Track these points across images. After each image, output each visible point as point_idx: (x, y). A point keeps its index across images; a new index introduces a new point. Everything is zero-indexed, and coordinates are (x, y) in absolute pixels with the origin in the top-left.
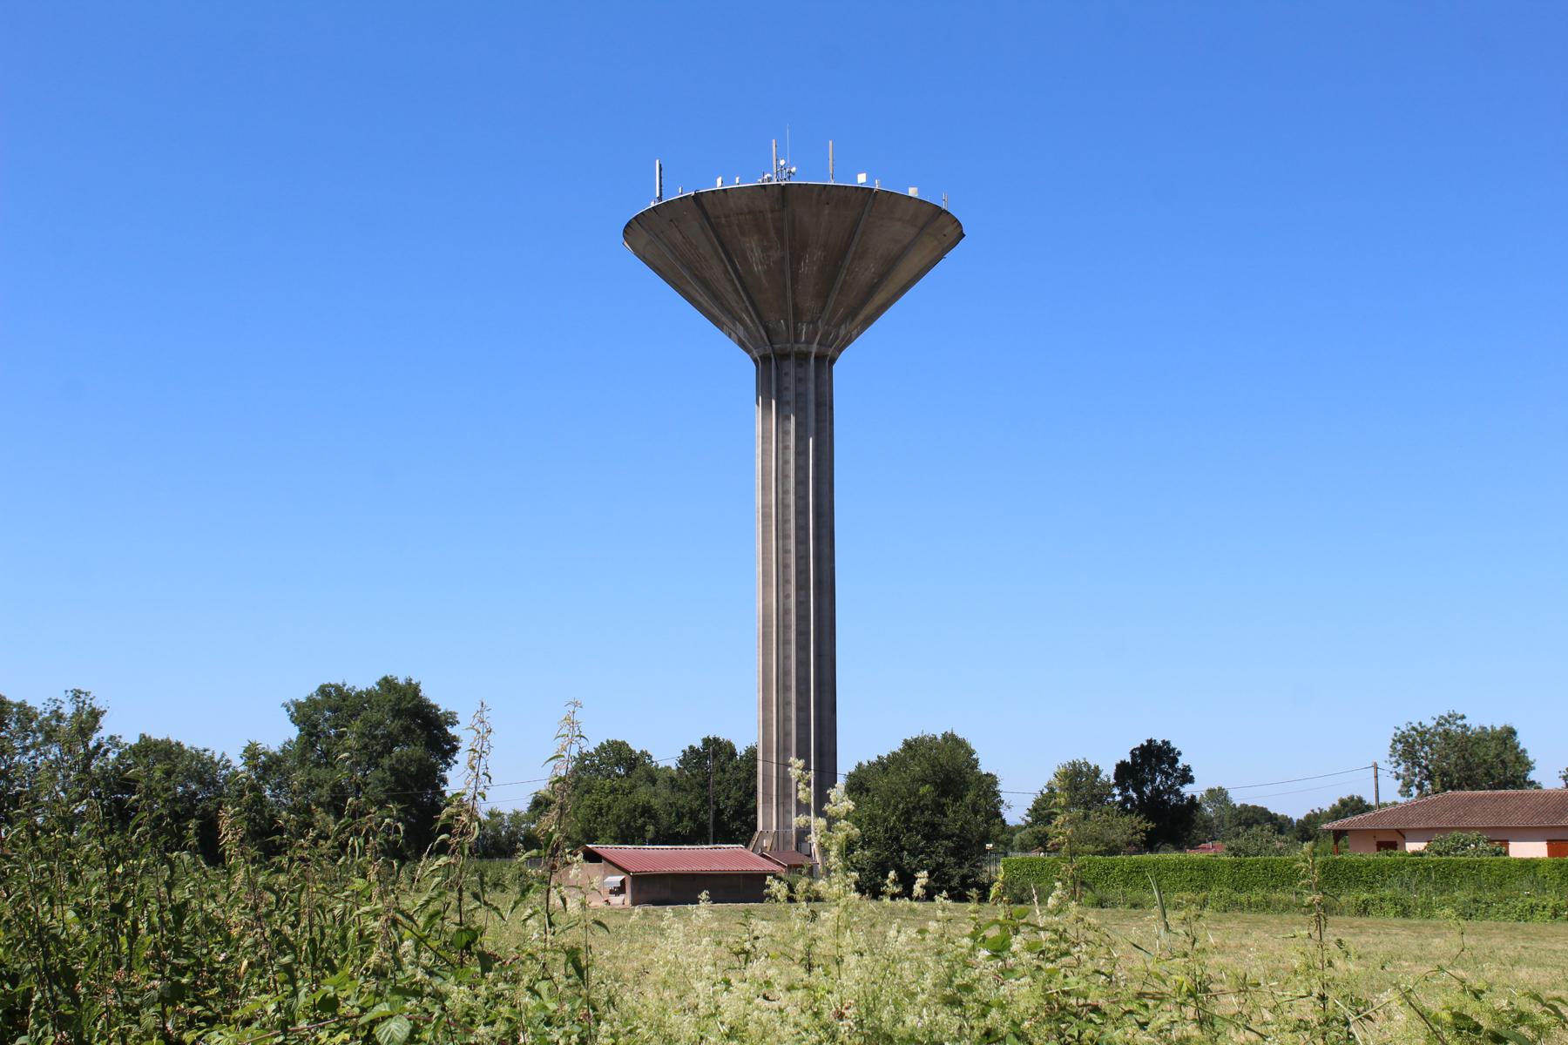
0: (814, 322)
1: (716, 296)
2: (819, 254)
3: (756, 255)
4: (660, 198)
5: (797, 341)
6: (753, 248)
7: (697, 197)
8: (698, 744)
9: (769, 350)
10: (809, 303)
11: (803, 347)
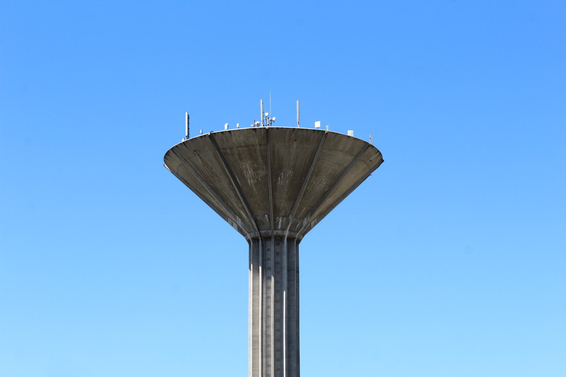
0: (286, 216)
1: (224, 200)
3: (249, 173)
4: (188, 137)
5: (275, 229)
7: (212, 136)
10: (283, 204)
11: (280, 232)
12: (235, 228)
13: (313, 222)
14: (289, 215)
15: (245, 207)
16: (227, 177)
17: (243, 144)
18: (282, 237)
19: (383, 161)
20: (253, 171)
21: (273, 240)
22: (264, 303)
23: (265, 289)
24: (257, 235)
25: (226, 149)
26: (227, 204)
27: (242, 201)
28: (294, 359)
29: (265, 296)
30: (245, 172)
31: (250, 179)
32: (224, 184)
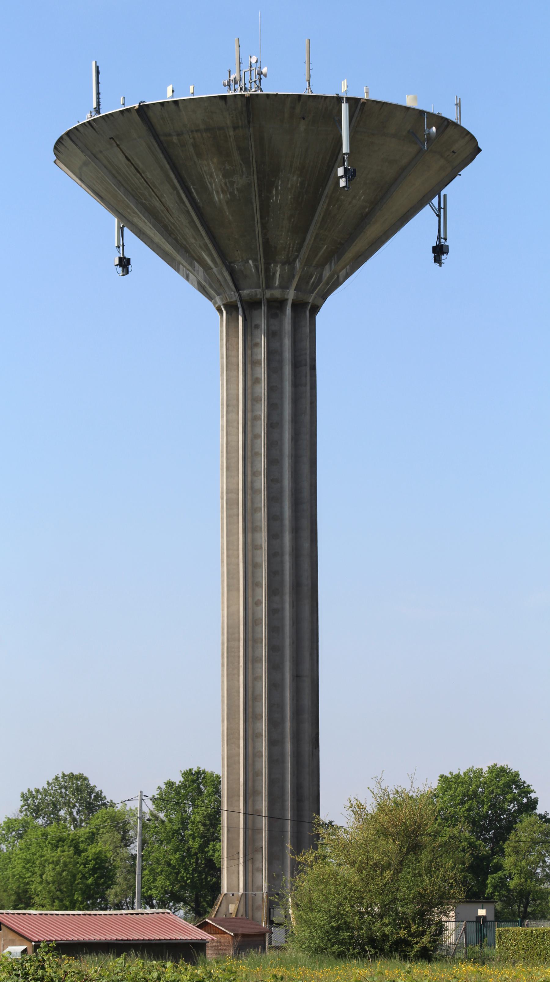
0: (290, 262)
1: (167, 231)
2: (295, 179)
3: (215, 182)
4: (98, 110)
5: (269, 285)
6: (212, 173)
7: (143, 110)
8: (178, 779)
9: (234, 297)
10: (283, 238)
11: (277, 293)
12: (194, 286)
13: (343, 272)
14: (294, 261)
15: (210, 246)
16: (175, 188)
17: (202, 127)
18: (282, 303)
19: (479, 150)
20: (224, 176)
21: (264, 308)
22: (249, 429)
23: (249, 402)
24: (234, 299)
25: (170, 135)
26: (176, 239)
27: (204, 234)
28: (305, 534)
29: (249, 415)
30: (207, 179)
31: (217, 192)
32: (169, 197)
